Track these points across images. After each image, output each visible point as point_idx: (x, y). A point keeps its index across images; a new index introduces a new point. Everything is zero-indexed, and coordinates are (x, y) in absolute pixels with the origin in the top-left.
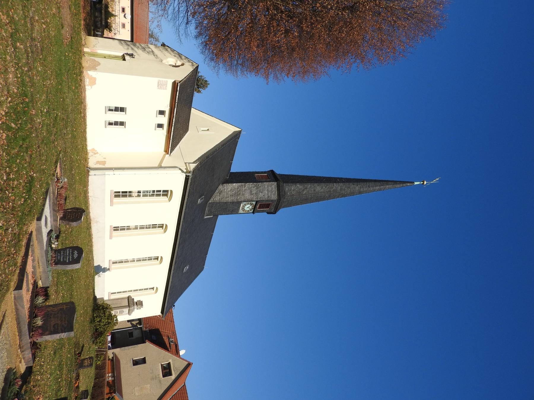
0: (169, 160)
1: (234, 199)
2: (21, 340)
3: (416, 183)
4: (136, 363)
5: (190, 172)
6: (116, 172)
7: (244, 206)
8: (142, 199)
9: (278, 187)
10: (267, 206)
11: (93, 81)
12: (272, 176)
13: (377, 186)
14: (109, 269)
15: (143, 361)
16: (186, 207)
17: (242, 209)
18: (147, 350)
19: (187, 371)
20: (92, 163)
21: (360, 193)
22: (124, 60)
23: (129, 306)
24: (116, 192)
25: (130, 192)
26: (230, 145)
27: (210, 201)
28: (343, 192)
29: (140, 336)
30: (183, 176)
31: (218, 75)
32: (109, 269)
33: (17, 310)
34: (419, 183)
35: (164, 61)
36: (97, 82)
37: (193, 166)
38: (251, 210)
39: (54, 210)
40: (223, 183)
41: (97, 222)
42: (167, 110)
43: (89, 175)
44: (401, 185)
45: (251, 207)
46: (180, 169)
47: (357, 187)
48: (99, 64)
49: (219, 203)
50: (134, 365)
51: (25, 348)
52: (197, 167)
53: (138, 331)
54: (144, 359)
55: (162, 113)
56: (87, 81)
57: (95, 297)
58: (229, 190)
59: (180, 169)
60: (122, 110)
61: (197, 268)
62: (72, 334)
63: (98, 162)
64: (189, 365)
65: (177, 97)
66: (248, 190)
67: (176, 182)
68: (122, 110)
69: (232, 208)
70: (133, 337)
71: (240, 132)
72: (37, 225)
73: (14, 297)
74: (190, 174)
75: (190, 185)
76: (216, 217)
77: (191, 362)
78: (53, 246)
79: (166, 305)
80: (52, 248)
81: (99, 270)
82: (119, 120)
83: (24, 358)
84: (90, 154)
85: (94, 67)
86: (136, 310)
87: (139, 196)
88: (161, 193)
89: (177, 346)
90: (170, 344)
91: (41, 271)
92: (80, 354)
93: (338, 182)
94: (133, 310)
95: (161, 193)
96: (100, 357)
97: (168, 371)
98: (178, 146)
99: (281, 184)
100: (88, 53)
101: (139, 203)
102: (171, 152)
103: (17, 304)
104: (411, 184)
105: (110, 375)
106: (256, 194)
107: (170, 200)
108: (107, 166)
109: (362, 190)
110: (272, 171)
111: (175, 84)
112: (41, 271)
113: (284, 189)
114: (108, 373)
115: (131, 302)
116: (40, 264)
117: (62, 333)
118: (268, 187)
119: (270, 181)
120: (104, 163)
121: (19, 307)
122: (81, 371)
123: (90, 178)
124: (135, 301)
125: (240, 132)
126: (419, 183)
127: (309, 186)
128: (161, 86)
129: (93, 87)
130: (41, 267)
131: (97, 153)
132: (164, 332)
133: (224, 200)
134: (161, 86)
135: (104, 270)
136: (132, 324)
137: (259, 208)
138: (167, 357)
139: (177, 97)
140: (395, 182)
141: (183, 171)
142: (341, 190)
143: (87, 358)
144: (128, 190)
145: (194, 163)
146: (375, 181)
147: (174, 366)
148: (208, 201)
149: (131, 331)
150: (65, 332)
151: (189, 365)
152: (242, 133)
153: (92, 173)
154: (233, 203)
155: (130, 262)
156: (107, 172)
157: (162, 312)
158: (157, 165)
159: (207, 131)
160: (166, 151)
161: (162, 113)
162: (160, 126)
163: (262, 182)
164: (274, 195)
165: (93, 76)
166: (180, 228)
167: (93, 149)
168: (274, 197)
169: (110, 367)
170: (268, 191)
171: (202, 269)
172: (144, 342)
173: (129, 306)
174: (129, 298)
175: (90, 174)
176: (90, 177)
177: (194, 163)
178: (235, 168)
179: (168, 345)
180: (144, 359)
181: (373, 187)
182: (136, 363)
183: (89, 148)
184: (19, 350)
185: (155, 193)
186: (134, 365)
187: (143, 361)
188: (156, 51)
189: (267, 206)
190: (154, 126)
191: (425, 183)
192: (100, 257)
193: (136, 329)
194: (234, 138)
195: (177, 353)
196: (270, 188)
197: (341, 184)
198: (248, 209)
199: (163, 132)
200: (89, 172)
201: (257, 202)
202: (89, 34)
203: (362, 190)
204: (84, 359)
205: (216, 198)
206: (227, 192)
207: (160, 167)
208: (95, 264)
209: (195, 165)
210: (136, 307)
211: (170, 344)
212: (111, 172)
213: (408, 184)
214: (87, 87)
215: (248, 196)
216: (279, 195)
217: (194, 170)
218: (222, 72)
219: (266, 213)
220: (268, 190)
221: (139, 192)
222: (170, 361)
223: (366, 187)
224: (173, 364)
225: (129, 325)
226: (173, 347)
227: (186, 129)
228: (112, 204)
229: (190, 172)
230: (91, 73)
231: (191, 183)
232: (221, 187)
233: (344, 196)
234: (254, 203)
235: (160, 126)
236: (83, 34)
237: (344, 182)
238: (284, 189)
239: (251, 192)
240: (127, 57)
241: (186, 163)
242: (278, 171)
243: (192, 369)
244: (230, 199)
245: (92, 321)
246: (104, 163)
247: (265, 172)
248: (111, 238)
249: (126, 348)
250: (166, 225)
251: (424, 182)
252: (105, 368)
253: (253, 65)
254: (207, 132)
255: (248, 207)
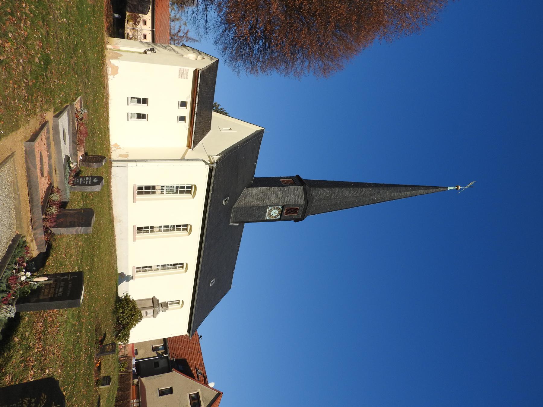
0: (191, 153)
1: (259, 203)
2: (32, 213)
3: (450, 188)
4: (162, 393)
5: (213, 163)
6: (139, 164)
7: (270, 212)
8: (163, 234)
9: (305, 191)
10: (295, 211)
11: (116, 70)
12: (298, 180)
13: (409, 191)
14: (133, 278)
15: (170, 391)
16: (211, 203)
17: (269, 214)
18: (174, 379)
19: (218, 401)
20: (114, 156)
21: (391, 199)
22: (146, 54)
23: (154, 307)
24: (137, 268)
25: (152, 227)
26: (252, 143)
27: (235, 206)
28: (373, 197)
29: (166, 365)
30: (208, 167)
31: (238, 75)
32: (133, 278)
33: (28, 169)
34: (452, 188)
35: (185, 56)
36: (119, 71)
37: (216, 158)
38: (278, 216)
39: (74, 142)
40: (248, 187)
41: (120, 221)
42: (189, 101)
43: (111, 167)
44: (434, 190)
45: (277, 212)
46: (203, 161)
47: (387, 193)
48: (122, 55)
49: (245, 207)
50: (160, 395)
51: (36, 224)
52: (220, 158)
53: (164, 360)
54: (171, 388)
55: (183, 104)
56: (110, 70)
57: (118, 297)
58: (254, 194)
59: (203, 161)
60: (144, 101)
61: (224, 286)
62: (90, 229)
63: (120, 156)
64: (219, 394)
65: (198, 87)
66: (273, 193)
67: (199, 176)
68: (144, 101)
69: (257, 215)
70: (158, 366)
71: (263, 131)
72: (54, 122)
73: (25, 150)
74: (214, 165)
75: (214, 179)
76: (242, 223)
77: (221, 391)
78: (72, 165)
79: (193, 321)
80: (70, 167)
81: (123, 278)
82: (141, 112)
83: (35, 240)
84: (113, 149)
85: (117, 57)
86: (161, 312)
87: (160, 231)
88: (185, 190)
89: (205, 378)
90: (198, 375)
91: (58, 180)
92: (102, 341)
93: (367, 187)
94: (158, 313)
95: (185, 190)
96: (124, 363)
97: (196, 401)
98: (200, 143)
99: (308, 188)
100: (110, 49)
101: (163, 199)
102: (194, 147)
103: (29, 162)
104: (444, 189)
105: (135, 401)
106: (283, 198)
107: (194, 197)
108: (129, 158)
109: (393, 195)
110: (298, 176)
111: (196, 72)
112: (58, 180)
113: (309, 197)
114: (133, 399)
115: (155, 303)
116: (57, 172)
117: (79, 226)
118: (294, 190)
119: (296, 185)
120: (127, 156)
121: (30, 165)
122: (104, 358)
123: (113, 170)
124: (160, 302)
125: (262, 131)
126: (452, 188)
127: (337, 190)
128: (182, 74)
129: (116, 76)
130: (58, 176)
131: (120, 148)
132: (192, 362)
133: (251, 204)
134: (182, 74)
135: (128, 278)
136: (157, 353)
137: (286, 213)
138: (196, 387)
139: (198, 87)
140: (427, 187)
141: (206, 163)
142: (371, 194)
143: (109, 344)
144: (149, 226)
145: (217, 155)
146: (406, 186)
147: (203, 396)
148: (234, 205)
149: (157, 361)
150: (82, 227)
151: (219, 394)
152: (265, 132)
153: (114, 164)
154: (259, 207)
155: (154, 255)
156: (130, 164)
157: (189, 331)
158: (180, 158)
159: (228, 131)
160: (189, 146)
161: (183, 104)
162: (182, 119)
163: (288, 186)
164: (301, 198)
165: (116, 65)
166: (205, 228)
167: (116, 145)
168: (302, 201)
169: (134, 390)
170: (295, 196)
171: (229, 288)
172: (170, 371)
173: (154, 307)
174: (153, 299)
175: (113, 165)
176: (113, 169)
177: (217, 155)
178: (259, 173)
179: (196, 377)
180: (171, 388)
181: (404, 191)
182: (162, 393)
183: (112, 143)
184: (31, 227)
185: (179, 190)
186: (160, 395)
187: (170, 391)
188: (176, 49)
189: (295, 211)
190: (176, 118)
191: (459, 188)
192: (124, 265)
193: (162, 358)
194: (257, 137)
195: (206, 383)
196: (296, 192)
197: (371, 189)
198: (275, 215)
199: (185, 125)
200: (111, 163)
201: (283, 206)
202: (111, 36)
203: (393, 195)
204: (106, 345)
205: (241, 202)
206: (252, 196)
207: (183, 159)
208: (119, 272)
209: (219, 157)
210: (161, 308)
211: (198, 375)
212: (133, 164)
213: (442, 189)
214: (110, 77)
215: (273, 200)
216: (306, 199)
217: (218, 161)
218: (243, 72)
219: (293, 221)
220: (294, 194)
221: (160, 227)
222: (199, 390)
223: (397, 192)
224: (202, 394)
225: (154, 354)
226: (202, 379)
227: (208, 128)
228: (135, 201)
229: (213, 163)
230: (114, 62)
231: (215, 176)
232: (245, 191)
233: (374, 202)
234: (281, 207)
235: (182, 119)
236: (105, 34)
237: (373, 187)
238: (309, 197)
239: (277, 195)
240: (148, 52)
241: (209, 156)
242: (304, 176)
243: (223, 398)
244: (255, 203)
245: (115, 312)
246: (127, 156)
247: (290, 177)
248: (134, 240)
249: (152, 377)
250: (191, 226)
251: (458, 187)
252: (129, 390)
253: (271, 63)
254: (231, 131)
255: (275, 213)
